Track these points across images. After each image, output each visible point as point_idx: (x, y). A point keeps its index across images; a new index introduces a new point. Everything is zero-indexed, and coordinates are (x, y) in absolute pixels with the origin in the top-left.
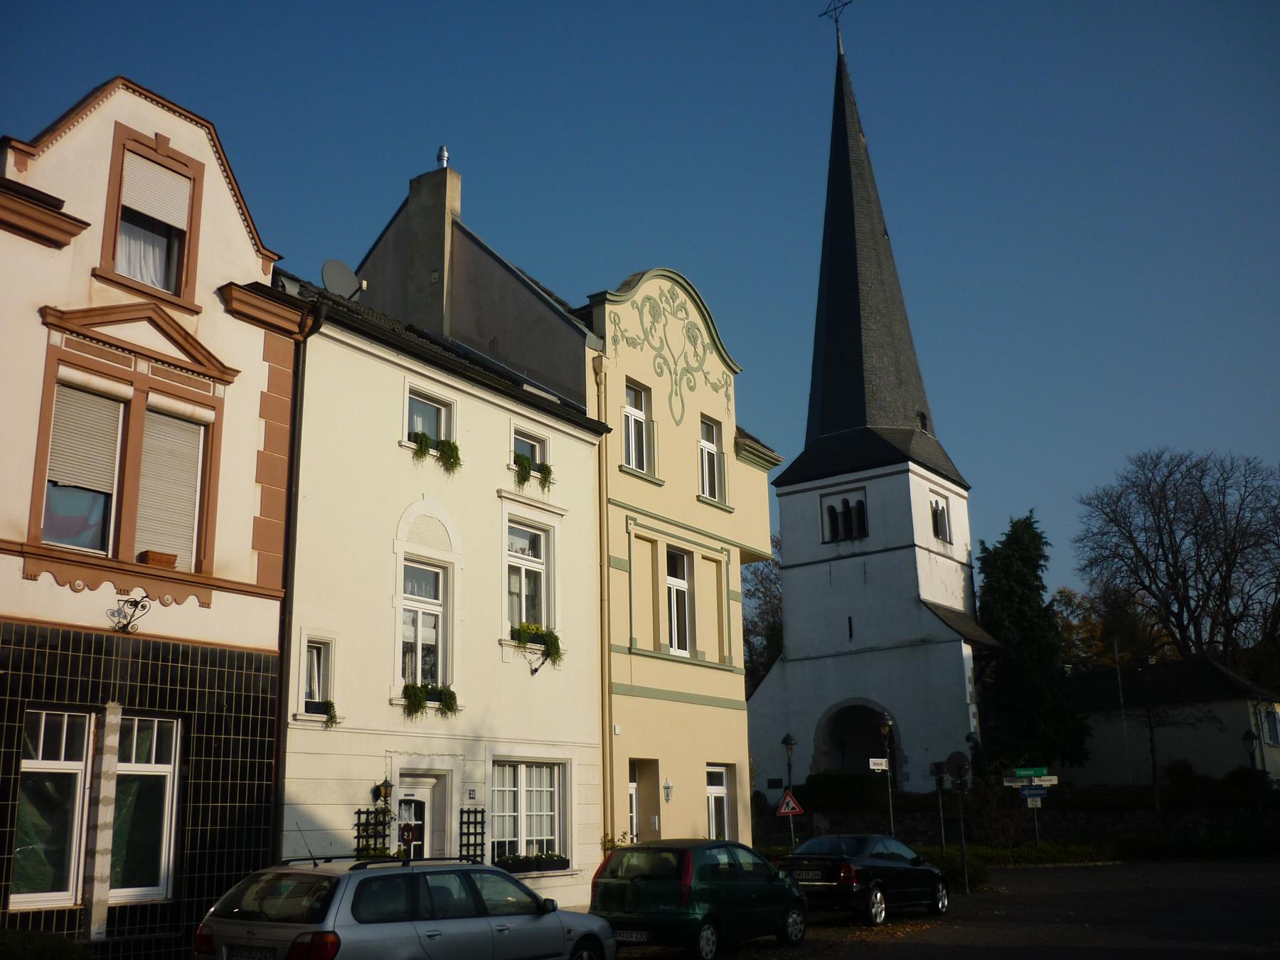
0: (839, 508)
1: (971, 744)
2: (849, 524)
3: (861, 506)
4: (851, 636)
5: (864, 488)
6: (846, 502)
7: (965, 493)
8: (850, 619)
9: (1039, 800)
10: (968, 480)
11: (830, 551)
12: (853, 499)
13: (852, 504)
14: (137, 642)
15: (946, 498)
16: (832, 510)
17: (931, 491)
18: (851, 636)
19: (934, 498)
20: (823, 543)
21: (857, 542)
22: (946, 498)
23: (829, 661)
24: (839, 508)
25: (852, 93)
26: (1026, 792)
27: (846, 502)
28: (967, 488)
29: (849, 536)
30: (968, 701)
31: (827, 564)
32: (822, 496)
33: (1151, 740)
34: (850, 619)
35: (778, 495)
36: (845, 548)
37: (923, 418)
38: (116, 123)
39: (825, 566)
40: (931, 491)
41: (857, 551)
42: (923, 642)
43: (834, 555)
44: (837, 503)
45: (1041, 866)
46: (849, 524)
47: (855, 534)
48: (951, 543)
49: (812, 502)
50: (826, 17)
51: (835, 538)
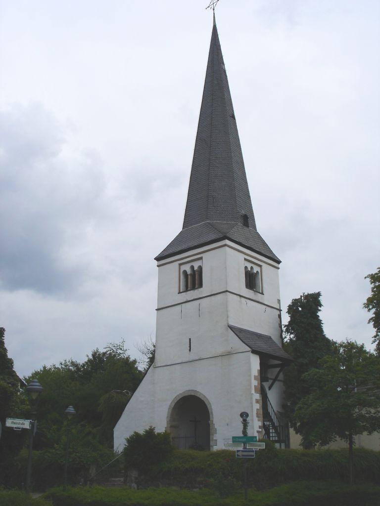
2: (193, 280)
3: (200, 268)
4: (190, 350)
6: (192, 267)
8: (190, 339)
11: (182, 271)
12: (196, 265)
13: (196, 268)
14: (171, 427)
15: (260, 266)
16: (185, 272)
17: (245, 259)
18: (190, 350)
19: (249, 265)
20: (179, 293)
21: (196, 291)
22: (260, 266)
23: (176, 366)
24: (189, 271)
25: (184, 392)
27: (192, 267)
29: (194, 288)
30: (253, 392)
31: (180, 306)
34: (190, 339)
35: (158, 266)
38: (155, 259)
39: (178, 308)
40: (245, 259)
44: (187, 268)
46: (193, 280)
48: (262, 294)
49: (173, 270)
51: (187, 290)
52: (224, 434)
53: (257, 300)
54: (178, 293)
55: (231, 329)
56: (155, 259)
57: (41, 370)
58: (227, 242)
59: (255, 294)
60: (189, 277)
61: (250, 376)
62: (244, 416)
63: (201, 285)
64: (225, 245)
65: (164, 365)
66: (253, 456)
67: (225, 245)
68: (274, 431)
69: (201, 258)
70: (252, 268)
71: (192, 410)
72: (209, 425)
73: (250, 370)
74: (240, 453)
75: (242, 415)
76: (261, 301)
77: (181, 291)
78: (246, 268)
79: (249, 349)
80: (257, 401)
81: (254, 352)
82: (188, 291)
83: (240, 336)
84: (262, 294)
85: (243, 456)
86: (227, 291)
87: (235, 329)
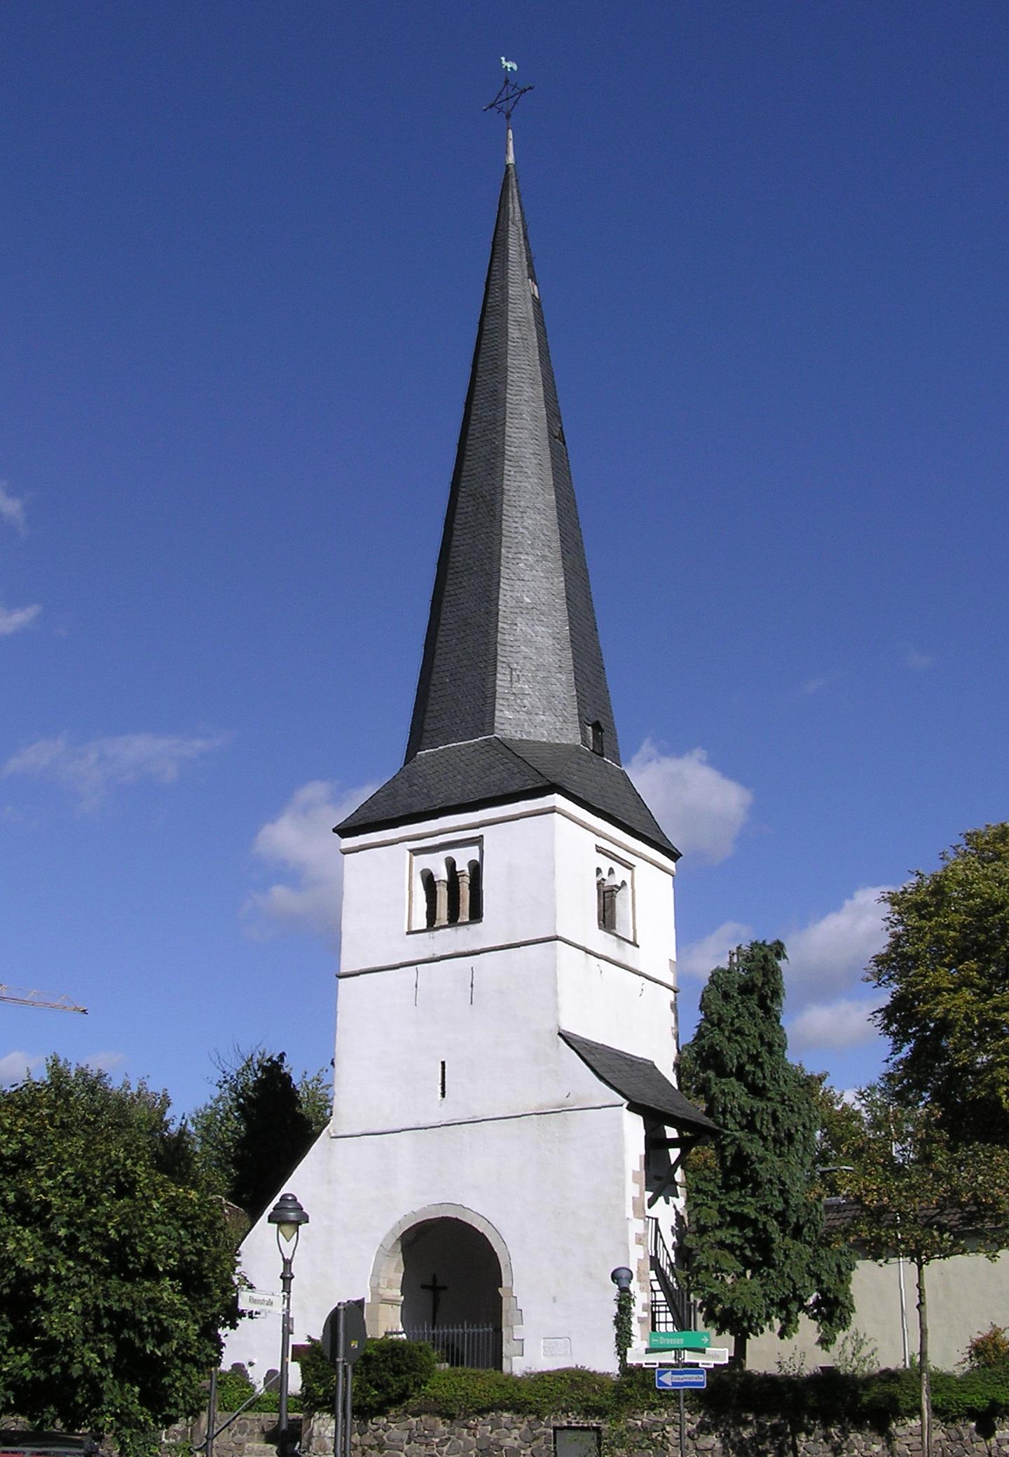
3: (476, 869)
4: (443, 1095)
5: (478, 841)
6: (451, 864)
7: (670, 865)
10: (676, 842)
13: (462, 866)
15: (630, 867)
17: (599, 850)
18: (443, 1095)
19: (606, 864)
21: (462, 930)
22: (630, 867)
27: (451, 864)
28: (673, 855)
30: (629, 1213)
32: (415, 852)
33: (920, 1286)
34: (443, 1063)
36: (449, 939)
37: (333, 1063)
38: (334, 830)
40: (599, 850)
42: (561, 1110)
45: (672, 1279)
47: (464, 916)
50: (522, 86)
52: (558, 1323)
53: (624, 962)
55: (567, 1042)
56: (334, 830)
57: (912, 1260)
58: (557, 800)
59: (619, 946)
61: (621, 1170)
62: (620, 1277)
63: (476, 914)
64: (553, 810)
65: (358, 1131)
66: (702, 1384)
67: (553, 810)
68: (670, 1318)
69: (478, 841)
70: (611, 871)
71: (452, 1266)
72: (499, 1299)
73: (619, 1152)
74: (668, 1379)
75: (615, 1276)
76: (631, 965)
78: (599, 871)
79: (622, 1100)
80: (639, 1241)
81: (633, 1107)
82: (437, 929)
83: (592, 1063)
84: (635, 944)
85: (674, 1384)
86: (557, 938)
87: (576, 1041)
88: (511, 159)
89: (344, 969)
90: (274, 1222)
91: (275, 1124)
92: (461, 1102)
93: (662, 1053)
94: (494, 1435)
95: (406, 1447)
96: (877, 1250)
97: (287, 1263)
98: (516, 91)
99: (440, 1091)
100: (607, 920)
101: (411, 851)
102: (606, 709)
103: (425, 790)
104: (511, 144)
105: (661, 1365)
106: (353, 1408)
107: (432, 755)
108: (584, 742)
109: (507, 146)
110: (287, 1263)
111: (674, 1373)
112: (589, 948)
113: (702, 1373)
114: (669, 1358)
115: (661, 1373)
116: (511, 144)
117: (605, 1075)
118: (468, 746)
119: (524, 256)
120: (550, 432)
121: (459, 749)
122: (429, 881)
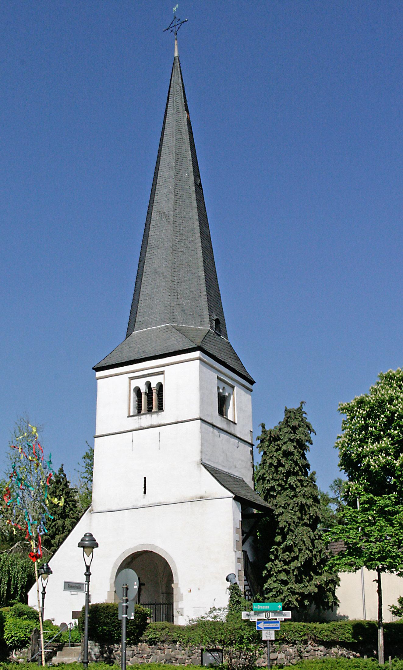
0: (143, 389)
1: (228, 584)
3: (160, 387)
4: (145, 493)
5: (162, 373)
6: (149, 384)
8: (145, 478)
9: (273, 632)
11: (135, 422)
12: (154, 381)
13: (153, 385)
16: (138, 391)
18: (145, 493)
19: (222, 385)
20: (129, 416)
21: (154, 416)
26: (261, 625)
27: (149, 384)
34: (145, 478)
36: (146, 420)
41: (155, 423)
43: (136, 426)
53: (229, 431)
54: (128, 417)
56: (93, 369)
60: (143, 396)
63: (160, 408)
65: (106, 509)
76: (233, 432)
77: (131, 414)
87: (209, 468)
88: (176, 54)
89: (97, 434)
90: (81, 547)
91: (66, 507)
92: (152, 497)
93: (247, 476)
94: (173, 653)
95: (131, 659)
96: (354, 567)
97: (88, 568)
98: (180, 22)
99: (143, 490)
100: (222, 411)
101: (129, 378)
102: (221, 313)
103: (137, 349)
104: (176, 47)
105: (258, 620)
106: (127, 632)
107: (140, 333)
108: (211, 327)
109: (174, 47)
110: (88, 568)
111: (265, 623)
112: (214, 424)
113: (278, 622)
114: (263, 616)
115: (258, 623)
116: (176, 47)
117: (223, 483)
118: (157, 329)
119: (183, 100)
120: (195, 183)
121: (153, 330)
122: (138, 391)
